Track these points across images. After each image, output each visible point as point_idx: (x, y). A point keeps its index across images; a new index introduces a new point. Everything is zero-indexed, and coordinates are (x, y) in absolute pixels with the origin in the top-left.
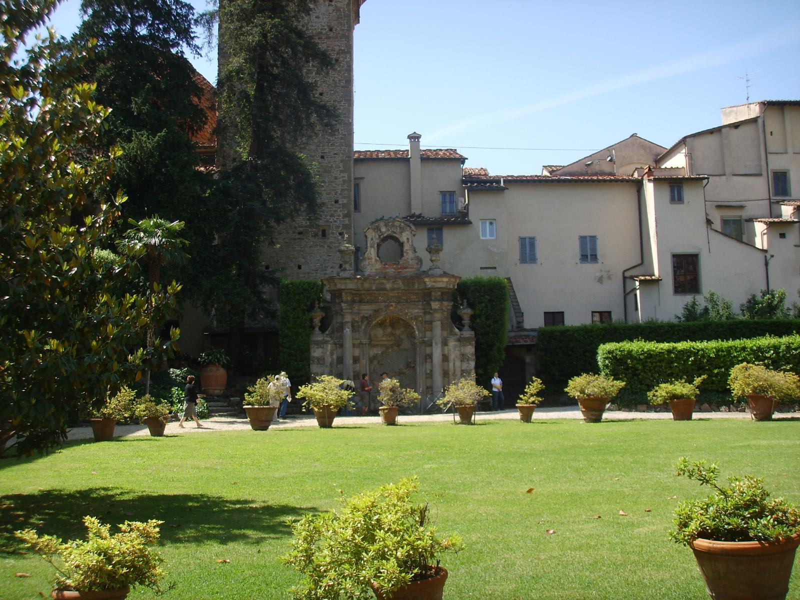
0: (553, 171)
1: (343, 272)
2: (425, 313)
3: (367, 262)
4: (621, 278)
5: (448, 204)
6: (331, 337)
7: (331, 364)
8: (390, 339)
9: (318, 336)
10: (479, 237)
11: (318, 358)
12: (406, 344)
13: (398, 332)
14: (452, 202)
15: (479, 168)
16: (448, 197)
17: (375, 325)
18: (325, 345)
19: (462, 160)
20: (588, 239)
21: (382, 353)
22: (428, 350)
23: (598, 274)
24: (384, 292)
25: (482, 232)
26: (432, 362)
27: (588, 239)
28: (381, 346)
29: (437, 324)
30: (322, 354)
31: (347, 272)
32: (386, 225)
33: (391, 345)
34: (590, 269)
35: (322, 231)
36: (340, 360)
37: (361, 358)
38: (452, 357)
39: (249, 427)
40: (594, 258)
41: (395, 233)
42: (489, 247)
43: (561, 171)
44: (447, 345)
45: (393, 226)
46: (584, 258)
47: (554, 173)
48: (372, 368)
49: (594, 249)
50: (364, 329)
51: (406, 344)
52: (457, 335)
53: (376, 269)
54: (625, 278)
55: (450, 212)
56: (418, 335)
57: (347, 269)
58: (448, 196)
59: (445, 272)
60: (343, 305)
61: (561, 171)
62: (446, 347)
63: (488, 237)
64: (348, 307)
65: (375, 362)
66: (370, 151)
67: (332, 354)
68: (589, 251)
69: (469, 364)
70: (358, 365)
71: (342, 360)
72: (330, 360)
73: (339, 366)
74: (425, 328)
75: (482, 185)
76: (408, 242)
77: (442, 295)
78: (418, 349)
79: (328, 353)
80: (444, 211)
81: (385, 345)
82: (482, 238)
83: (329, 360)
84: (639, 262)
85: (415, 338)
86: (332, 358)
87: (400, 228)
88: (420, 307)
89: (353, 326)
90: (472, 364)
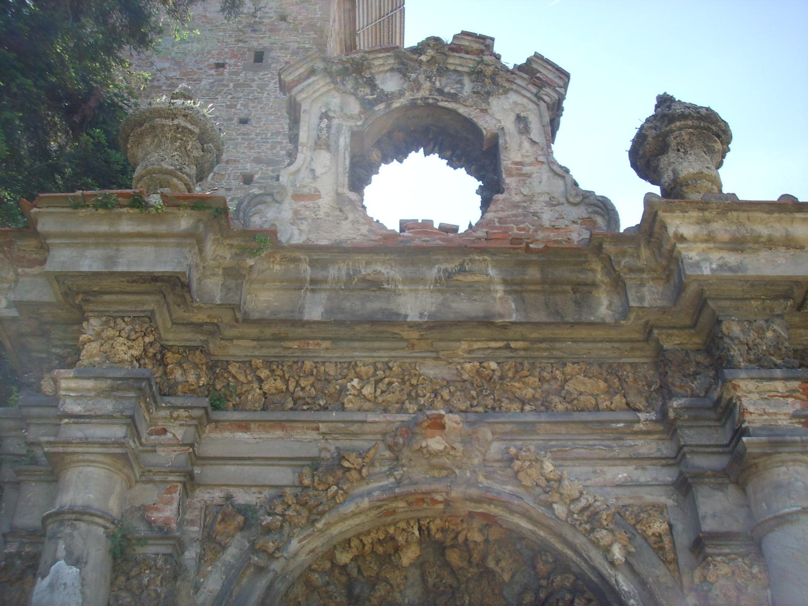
41: (454, 97)
64: (108, 406)
88: (646, 446)
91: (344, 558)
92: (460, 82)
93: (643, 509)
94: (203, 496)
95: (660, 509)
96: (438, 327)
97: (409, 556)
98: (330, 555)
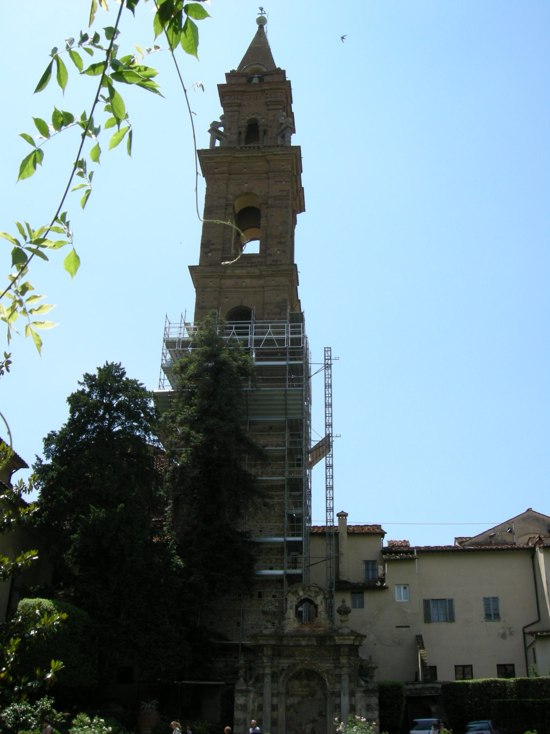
0: (463, 542)
2: (335, 667)
3: (286, 622)
4: (522, 634)
5: (370, 572)
6: (253, 687)
7: (253, 710)
9: (241, 685)
10: (394, 600)
11: (241, 706)
12: (319, 695)
13: (312, 684)
14: (375, 570)
15: (402, 540)
16: (370, 566)
17: (292, 677)
19: (382, 534)
20: (491, 599)
21: (298, 703)
22: (337, 701)
23: (501, 631)
26: (340, 711)
27: (491, 599)
29: (345, 678)
31: (268, 630)
32: (304, 590)
34: (495, 627)
36: (261, 708)
38: (359, 707)
40: (497, 616)
41: (311, 597)
42: (403, 608)
46: (488, 616)
47: (463, 544)
49: (497, 609)
51: (319, 695)
53: (294, 628)
54: (524, 634)
58: (370, 565)
59: (352, 631)
63: (403, 600)
64: (269, 661)
65: (292, 711)
66: (317, 526)
67: (254, 701)
68: (492, 611)
69: (373, 713)
70: (276, 713)
71: (262, 708)
72: (252, 707)
75: (402, 553)
76: (322, 604)
79: (251, 701)
80: (367, 577)
82: (397, 600)
83: (251, 707)
84: (537, 619)
85: (326, 689)
87: (315, 592)
88: (332, 662)
90: (377, 713)
96: (307, 646)
97: (303, 673)
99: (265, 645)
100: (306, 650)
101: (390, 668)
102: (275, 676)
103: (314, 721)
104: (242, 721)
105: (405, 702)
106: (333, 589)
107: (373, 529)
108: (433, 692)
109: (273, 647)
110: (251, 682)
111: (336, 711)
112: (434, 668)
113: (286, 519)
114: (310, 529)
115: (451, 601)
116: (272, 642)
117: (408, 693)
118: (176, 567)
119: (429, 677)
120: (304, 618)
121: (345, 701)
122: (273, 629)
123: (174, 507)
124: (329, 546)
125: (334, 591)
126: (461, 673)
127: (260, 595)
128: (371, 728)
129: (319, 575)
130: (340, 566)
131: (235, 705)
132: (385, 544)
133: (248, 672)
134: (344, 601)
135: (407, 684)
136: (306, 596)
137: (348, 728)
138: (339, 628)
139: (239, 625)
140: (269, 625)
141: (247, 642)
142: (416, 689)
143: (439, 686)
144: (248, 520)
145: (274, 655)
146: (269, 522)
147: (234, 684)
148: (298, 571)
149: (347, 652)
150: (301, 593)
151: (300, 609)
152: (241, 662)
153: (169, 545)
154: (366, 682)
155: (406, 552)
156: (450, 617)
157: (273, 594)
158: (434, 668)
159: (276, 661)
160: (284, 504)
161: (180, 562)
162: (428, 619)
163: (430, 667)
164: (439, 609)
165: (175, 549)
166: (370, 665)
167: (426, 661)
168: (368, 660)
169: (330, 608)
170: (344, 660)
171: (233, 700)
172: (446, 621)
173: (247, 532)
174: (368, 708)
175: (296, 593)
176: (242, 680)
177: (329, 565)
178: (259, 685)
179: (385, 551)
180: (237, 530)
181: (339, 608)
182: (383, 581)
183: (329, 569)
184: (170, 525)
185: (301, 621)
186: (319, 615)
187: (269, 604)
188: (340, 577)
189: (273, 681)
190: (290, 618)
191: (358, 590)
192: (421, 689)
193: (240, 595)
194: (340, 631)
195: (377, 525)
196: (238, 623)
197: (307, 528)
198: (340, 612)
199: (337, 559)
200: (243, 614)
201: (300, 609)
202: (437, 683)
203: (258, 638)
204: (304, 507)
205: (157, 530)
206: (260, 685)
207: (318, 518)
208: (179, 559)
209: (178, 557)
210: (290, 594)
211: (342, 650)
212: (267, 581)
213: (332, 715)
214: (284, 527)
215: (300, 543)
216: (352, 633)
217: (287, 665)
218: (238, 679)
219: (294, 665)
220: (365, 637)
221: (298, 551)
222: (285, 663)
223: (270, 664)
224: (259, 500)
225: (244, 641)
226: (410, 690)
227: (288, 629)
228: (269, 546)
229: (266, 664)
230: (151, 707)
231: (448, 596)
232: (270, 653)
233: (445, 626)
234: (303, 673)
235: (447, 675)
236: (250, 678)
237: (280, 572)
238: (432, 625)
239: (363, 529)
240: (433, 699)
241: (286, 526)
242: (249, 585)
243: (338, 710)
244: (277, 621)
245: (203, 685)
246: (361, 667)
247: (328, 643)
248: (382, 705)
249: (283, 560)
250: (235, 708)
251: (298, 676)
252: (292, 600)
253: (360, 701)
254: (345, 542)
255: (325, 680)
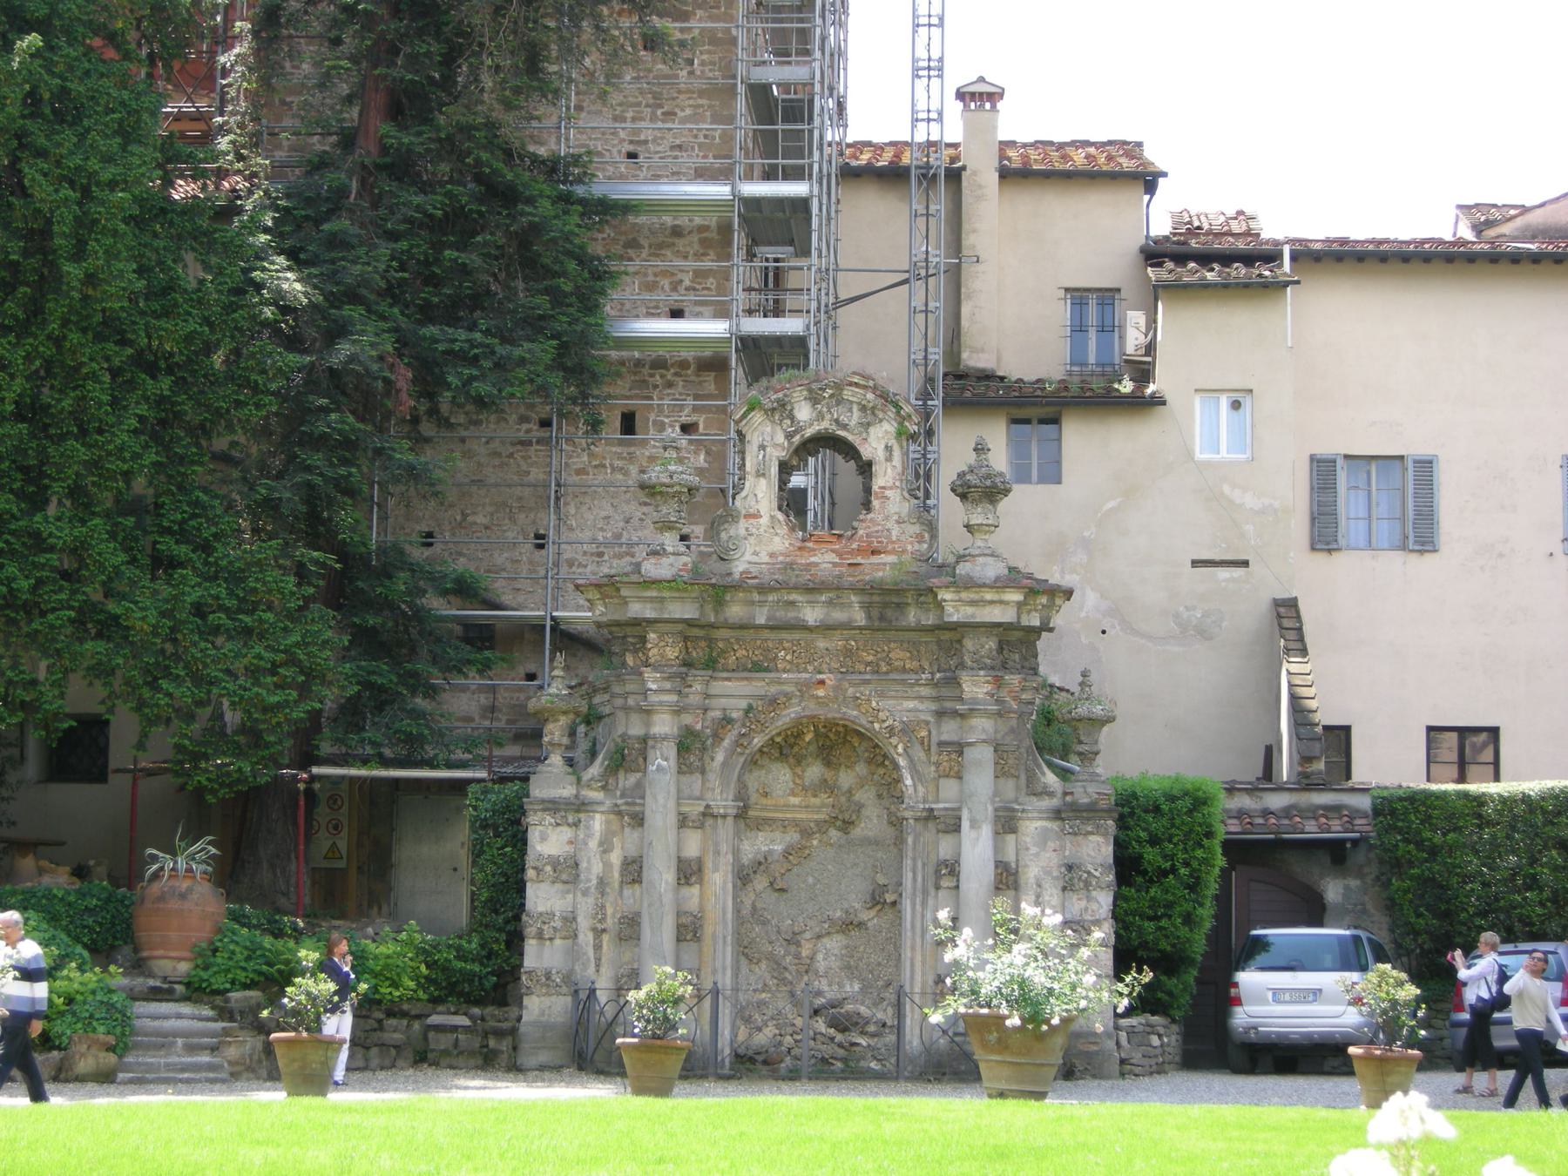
0: (1490, 224)
1: (653, 561)
2: (940, 714)
3: (741, 527)
5: (1092, 335)
6: (604, 788)
7: (602, 883)
8: (816, 801)
9: (551, 781)
10: (1190, 454)
11: (555, 863)
12: (872, 823)
13: (846, 779)
14: (1110, 329)
18: (582, 816)
19: (1148, 181)
21: (787, 853)
22: (945, 848)
24: (797, 635)
25: (1201, 429)
28: (784, 825)
30: (570, 849)
31: (665, 561)
32: (814, 399)
33: (817, 822)
35: (623, 415)
37: (709, 864)
38: (1031, 873)
39: (284, 1094)
42: (1226, 489)
43: (1519, 222)
44: (1014, 830)
45: (838, 403)
48: (748, 903)
50: (724, 764)
51: (872, 823)
52: (1051, 794)
53: (772, 555)
55: (1097, 365)
56: (911, 790)
57: (670, 549)
58: (1092, 306)
60: (648, 674)
61: (1519, 222)
62: (1010, 838)
63: (1224, 454)
64: (668, 685)
65: (760, 883)
66: (869, 144)
67: (606, 847)
70: (695, 890)
72: (597, 868)
73: (627, 892)
74: (938, 764)
75: (1221, 265)
76: (889, 459)
77: (1000, 649)
78: (910, 840)
79: (593, 844)
80: (1078, 359)
81: (796, 823)
82: (1200, 456)
83: (593, 867)
86: (607, 865)
87: (863, 408)
88: (925, 691)
89: (683, 748)
91: (778, 739)
92: (850, 410)
93: (918, 723)
94: (711, 714)
95: (927, 723)
96: (826, 628)
97: (808, 737)
98: (772, 739)
99: (651, 622)
100: (822, 644)
101: (1165, 723)
102: (689, 746)
103: (849, 925)
104: (558, 923)
105: (1220, 861)
106: (936, 403)
107: (1110, 158)
108: (1336, 825)
109: (688, 631)
110: (595, 770)
111: (938, 888)
112: (1340, 736)
113: (741, 104)
114: (841, 154)
115: (1426, 466)
116: (687, 611)
117: (1234, 826)
118: (276, 304)
119: (1321, 766)
120: (810, 516)
121: (976, 850)
122: (685, 559)
123: (256, 52)
124: (921, 221)
125: (939, 411)
126: (1454, 757)
127: (629, 423)
128: (1085, 953)
129: (878, 341)
130: (966, 310)
131: (530, 860)
132: (1161, 227)
133: (582, 729)
134: (980, 449)
135: (1231, 790)
136: (825, 425)
137: (993, 948)
138: (961, 558)
139: (540, 541)
140: (670, 541)
141: (579, 613)
142: (1266, 813)
143: (1364, 803)
144: (579, 108)
145: (688, 664)
146: (670, 114)
147: (525, 779)
148: (790, 325)
149: (995, 655)
150: (804, 412)
151: (797, 480)
152: (553, 690)
153: (239, 211)
154: (1064, 774)
155: (1249, 259)
156: (1420, 534)
157: (684, 419)
158: (1340, 736)
159: (698, 687)
160: (734, 41)
161: (293, 285)
162: (1324, 535)
163: (1326, 728)
164: (1377, 498)
165: (266, 230)
166: (1082, 710)
167: (1312, 704)
168: (1076, 689)
169: (920, 479)
170: (976, 687)
171: (520, 841)
172: (1403, 547)
173: (576, 160)
174: (1072, 878)
175: (782, 409)
176: (556, 760)
177: (918, 302)
178: (628, 780)
179: (1154, 254)
180: (531, 148)
181: (961, 475)
182: (1143, 373)
183: (921, 318)
184: (241, 126)
185: (803, 528)
186: (875, 503)
187: (668, 456)
188: (965, 355)
189: (684, 768)
190: (757, 516)
191: (1038, 408)
192: (1287, 812)
193: (545, 423)
194: (963, 569)
195: (1125, 143)
196: (538, 536)
197: (827, 150)
198: (963, 491)
199: (955, 276)
200: (557, 499)
201: (797, 480)
202: (1353, 790)
203: (624, 592)
204: (818, 54)
205: (187, 149)
206: (633, 779)
207: (877, 106)
208: (289, 269)
209: (281, 260)
210: (757, 417)
211: (969, 644)
212: (659, 364)
213: (924, 904)
214: (732, 138)
215: (801, 206)
216: (1013, 578)
217: (743, 704)
218: (541, 760)
219: (773, 702)
220: (1068, 594)
221: (791, 243)
222: (733, 694)
223: (674, 698)
224: (626, 23)
225: (565, 608)
226: (1240, 814)
227: (748, 557)
228: (668, 220)
229: (653, 698)
230: (189, 870)
231: (1412, 446)
232: (672, 653)
233: (1396, 566)
234: (808, 737)
235: (1389, 762)
236: (593, 754)
237: (715, 328)
238: (1342, 562)
239: (1065, 158)
240: (1336, 853)
241: (740, 135)
242: (580, 377)
243: (946, 882)
244: (698, 530)
245: (397, 781)
246: (1048, 718)
247: (912, 616)
248: (1127, 867)
249: (727, 279)
250: (530, 873)
251: (785, 748)
252: (767, 441)
253: (1039, 847)
254: (990, 211)
255: (896, 767)
